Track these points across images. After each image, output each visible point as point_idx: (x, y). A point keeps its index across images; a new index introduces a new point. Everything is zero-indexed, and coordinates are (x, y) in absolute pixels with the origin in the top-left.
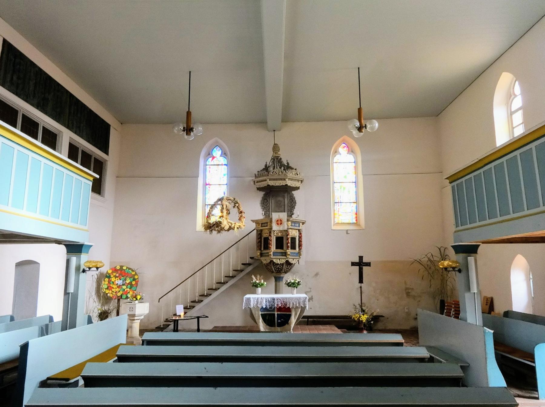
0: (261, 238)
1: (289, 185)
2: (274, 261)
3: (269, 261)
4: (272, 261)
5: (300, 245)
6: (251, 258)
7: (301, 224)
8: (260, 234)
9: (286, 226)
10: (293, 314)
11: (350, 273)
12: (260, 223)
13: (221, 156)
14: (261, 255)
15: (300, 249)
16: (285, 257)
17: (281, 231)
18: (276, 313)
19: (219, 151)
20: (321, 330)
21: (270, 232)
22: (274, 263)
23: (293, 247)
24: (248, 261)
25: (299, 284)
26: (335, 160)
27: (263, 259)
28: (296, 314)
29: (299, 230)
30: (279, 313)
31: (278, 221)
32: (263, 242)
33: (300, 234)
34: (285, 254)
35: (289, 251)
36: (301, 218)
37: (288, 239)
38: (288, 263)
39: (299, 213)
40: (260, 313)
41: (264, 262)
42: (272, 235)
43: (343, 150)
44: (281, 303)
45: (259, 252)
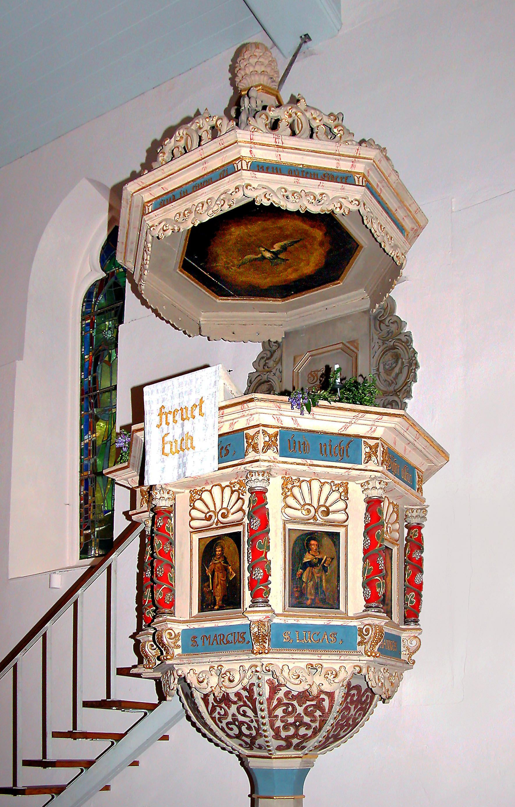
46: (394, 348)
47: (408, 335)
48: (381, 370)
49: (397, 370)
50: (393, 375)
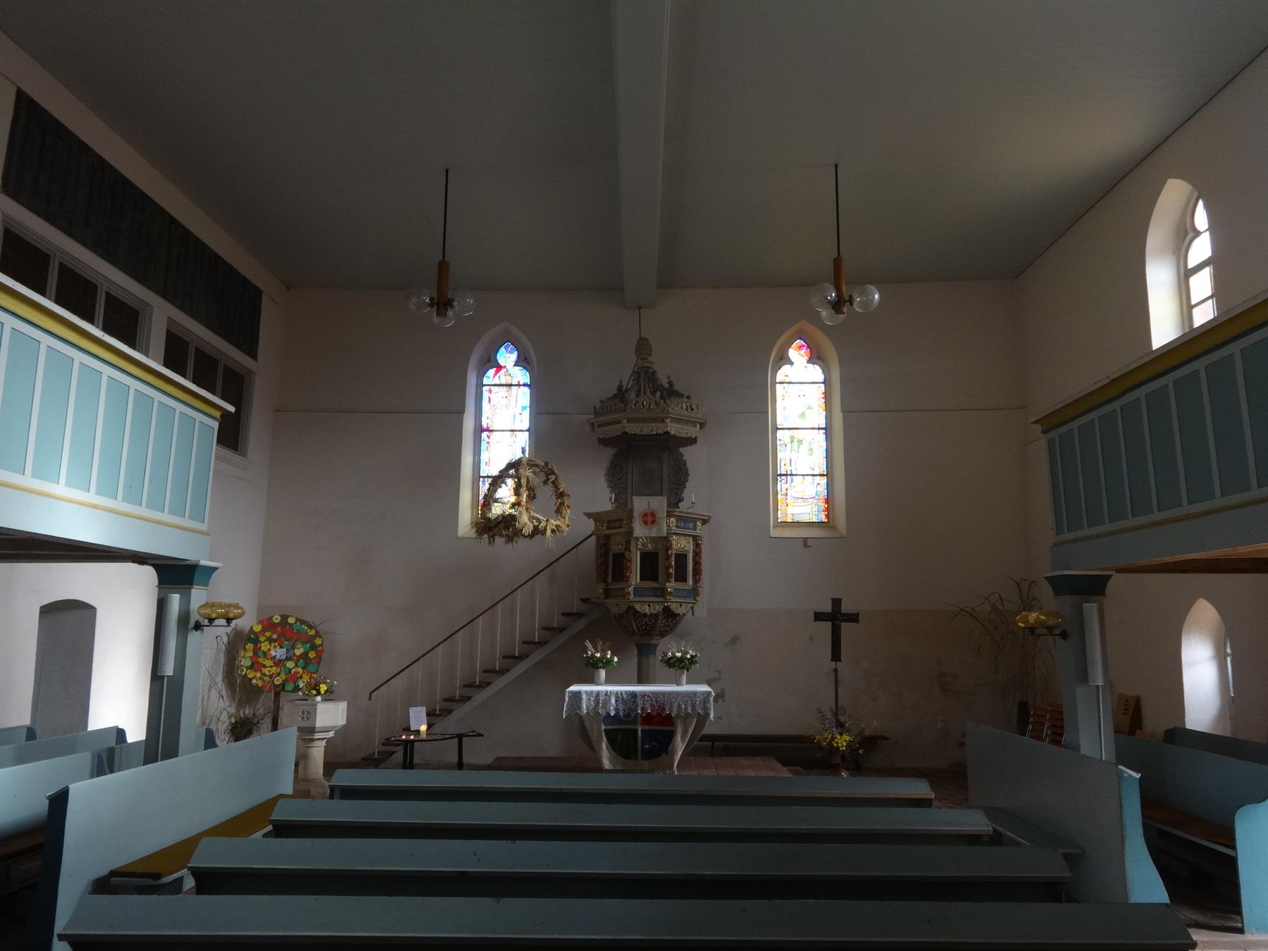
0: (606, 554)
2: (637, 607)
3: (624, 608)
5: (697, 572)
6: (582, 600)
8: (604, 545)
10: (679, 730)
11: (811, 639)
13: (516, 364)
14: (607, 593)
15: (696, 581)
21: (628, 542)
22: (636, 612)
23: (681, 577)
24: (576, 606)
26: (780, 376)
29: (695, 538)
30: (646, 727)
31: (645, 515)
33: (697, 546)
34: (662, 592)
35: (671, 586)
36: (700, 510)
37: (668, 557)
38: (669, 614)
39: (694, 498)
41: (614, 610)
43: (797, 354)
44: (652, 705)
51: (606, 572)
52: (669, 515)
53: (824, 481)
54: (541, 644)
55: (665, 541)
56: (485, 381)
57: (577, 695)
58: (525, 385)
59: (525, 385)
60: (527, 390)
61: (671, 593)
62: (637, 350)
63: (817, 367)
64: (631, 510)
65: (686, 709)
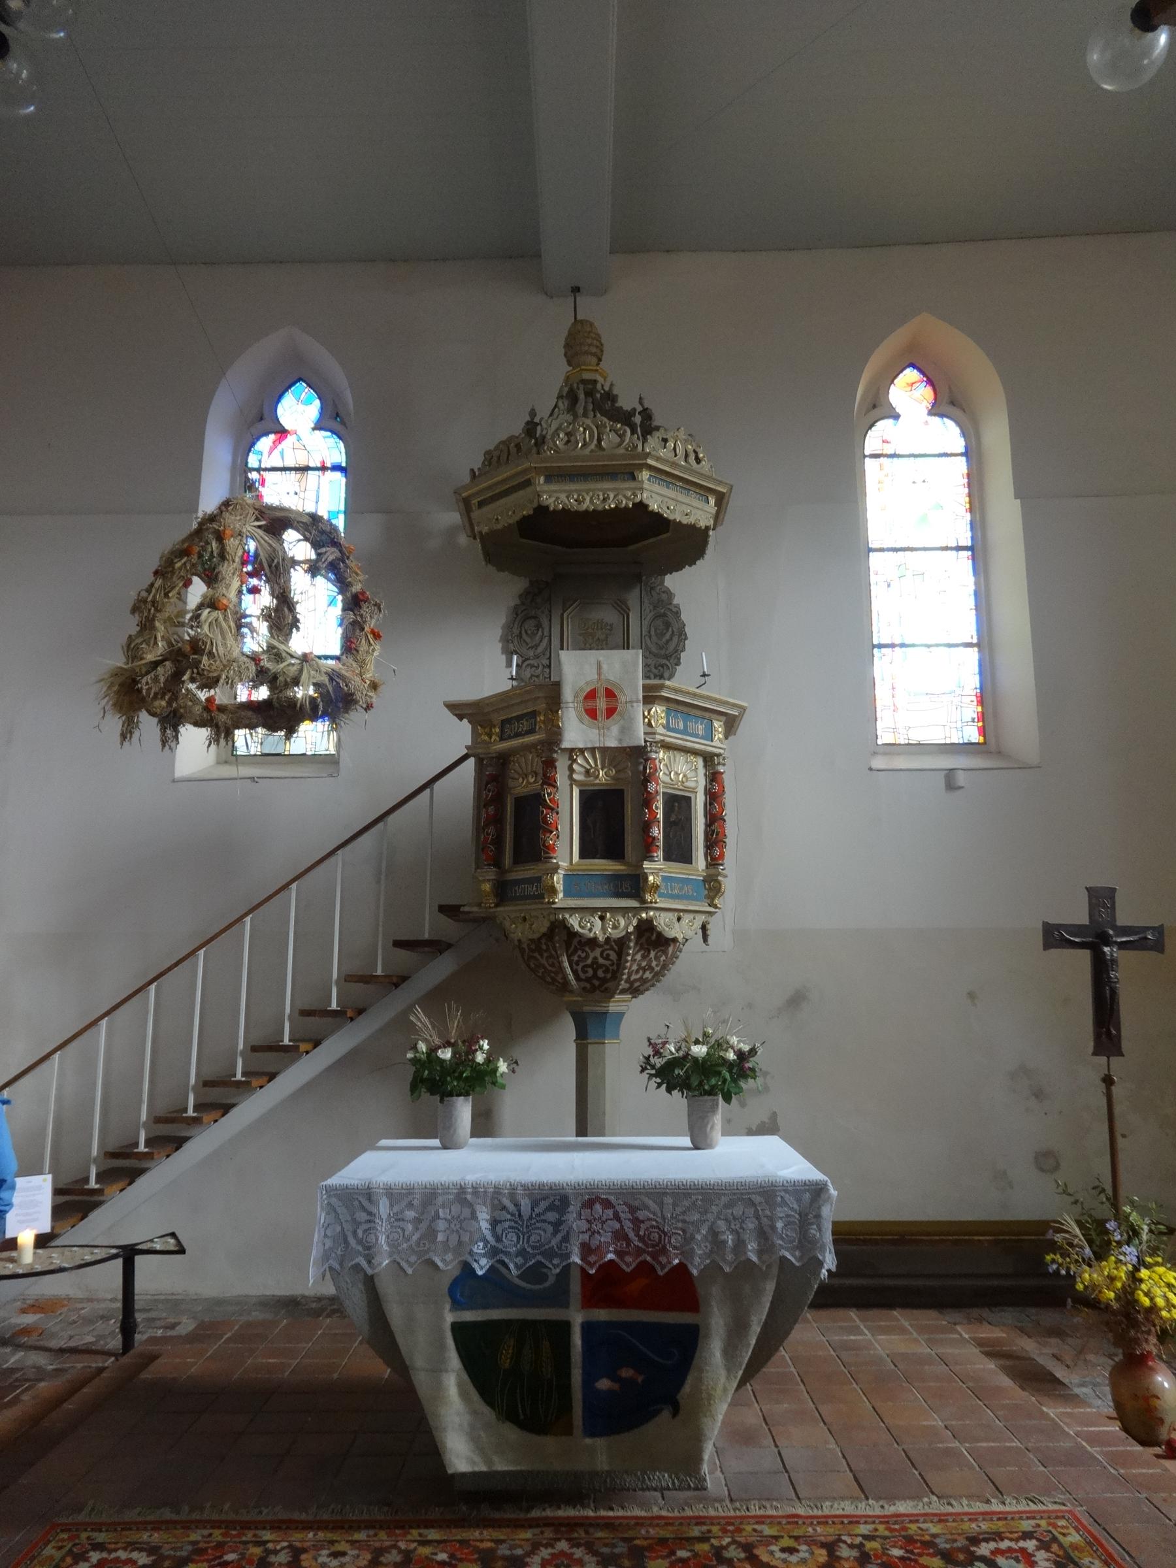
0: (498, 799)
1: (654, 507)
2: (574, 922)
3: (542, 927)
4: (564, 925)
5: (714, 840)
6: (442, 909)
7: (718, 726)
8: (494, 776)
9: (640, 730)
10: (717, 1323)
11: (971, 995)
12: (497, 718)
13: (318, 427)
14: (503, 891)
15: (714, 861)
16: (633, 903)
17: (611, 756)
18: (577, 1318)
19: (307, 403)
20: (856, 1330)
21: (550, 764)
22: (571, 934)
23: (679, 852)
24: (428, 926)
25: (742, 1067)
26: (873, 442)
27: (507, 913)
28: (738, 1328)
29: (709, 759)
30: (602, 1315)
31: (591, 695)
32: (509, 819)
33: (714, 777)
34: (633, 886)
35: (656, 869)
36: (717, 691)
37: (647, 802)
38: (651, 939)
39: (700, 668)
40: (449, 1318)
41: (519, 932)
42: (561, 778)
43: (909, 393)
44: (620, 1236)
45: (491, 873)
46: (664, 615)
47: (677, 606)
48: (653, 633)
49: (668, 636)
50: (664, 640)
51: (498, 841)
52: (649, 700)
53: (973, 655)
54: (342, 1017)
55: (634, 760)
56: (253, 461)
57: (359, 1200)
58: (336, 468)
59: (336, 468)
60: (339, 478)
61: (656, 888)
62: (567, 346)
63: (950, 424)
64: (557, 686)
65: (740, 1245)
